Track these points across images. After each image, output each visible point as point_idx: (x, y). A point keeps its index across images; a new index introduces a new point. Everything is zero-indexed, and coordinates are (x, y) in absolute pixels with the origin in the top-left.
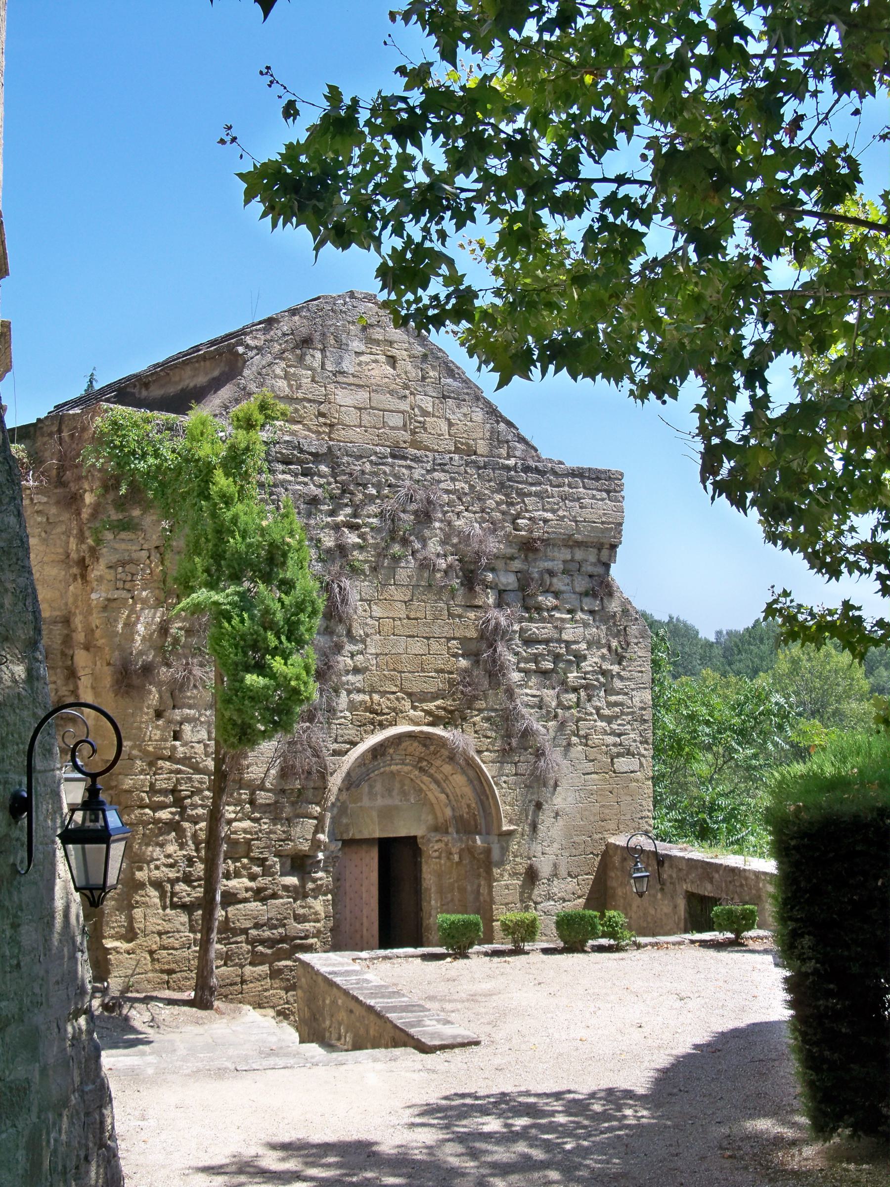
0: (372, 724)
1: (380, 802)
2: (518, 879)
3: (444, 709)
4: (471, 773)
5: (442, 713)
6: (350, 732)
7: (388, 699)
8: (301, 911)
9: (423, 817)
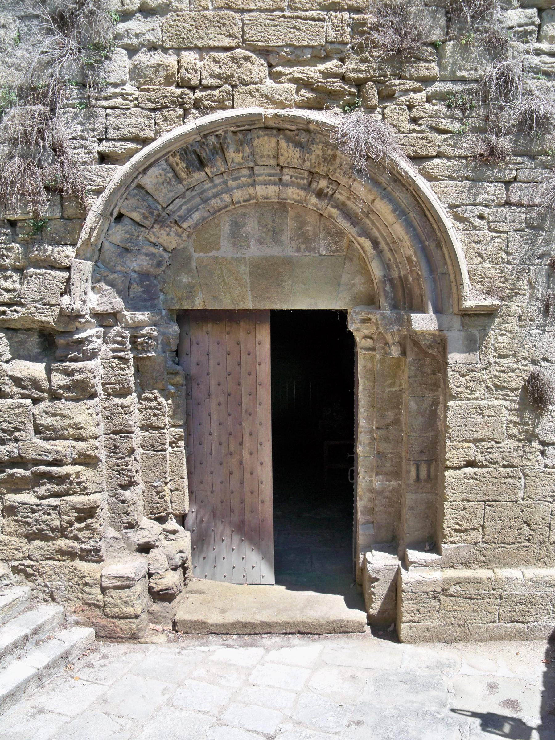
0: (181, 105)
1: (254, 251)
2: (506, 398)
3: (343, 78)
4: (400, 196)
5: (338, 85)
6: (134, 121)
7: (216, 61)
8: (47, 421)
9: (345, 278)
